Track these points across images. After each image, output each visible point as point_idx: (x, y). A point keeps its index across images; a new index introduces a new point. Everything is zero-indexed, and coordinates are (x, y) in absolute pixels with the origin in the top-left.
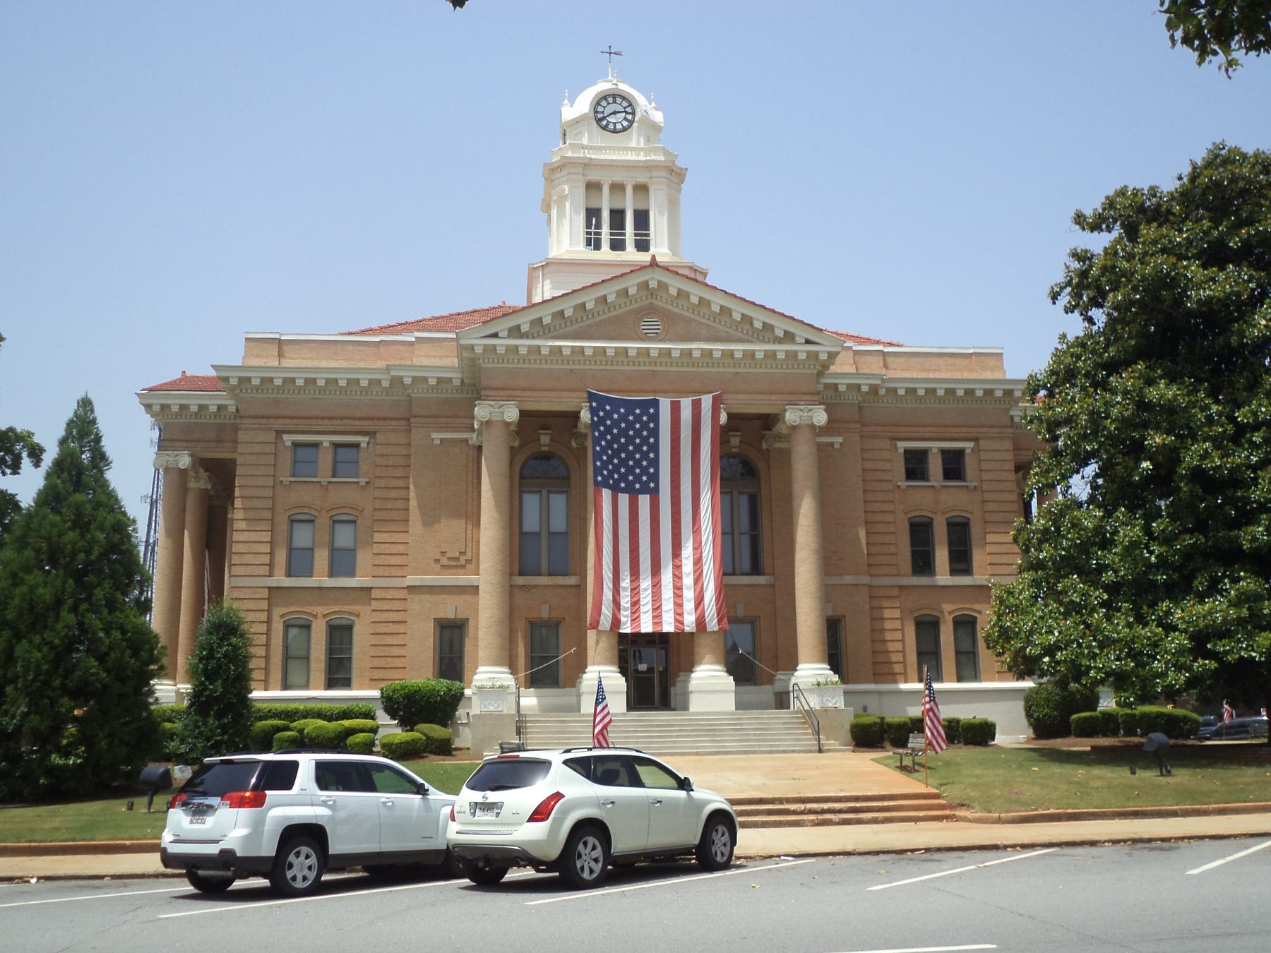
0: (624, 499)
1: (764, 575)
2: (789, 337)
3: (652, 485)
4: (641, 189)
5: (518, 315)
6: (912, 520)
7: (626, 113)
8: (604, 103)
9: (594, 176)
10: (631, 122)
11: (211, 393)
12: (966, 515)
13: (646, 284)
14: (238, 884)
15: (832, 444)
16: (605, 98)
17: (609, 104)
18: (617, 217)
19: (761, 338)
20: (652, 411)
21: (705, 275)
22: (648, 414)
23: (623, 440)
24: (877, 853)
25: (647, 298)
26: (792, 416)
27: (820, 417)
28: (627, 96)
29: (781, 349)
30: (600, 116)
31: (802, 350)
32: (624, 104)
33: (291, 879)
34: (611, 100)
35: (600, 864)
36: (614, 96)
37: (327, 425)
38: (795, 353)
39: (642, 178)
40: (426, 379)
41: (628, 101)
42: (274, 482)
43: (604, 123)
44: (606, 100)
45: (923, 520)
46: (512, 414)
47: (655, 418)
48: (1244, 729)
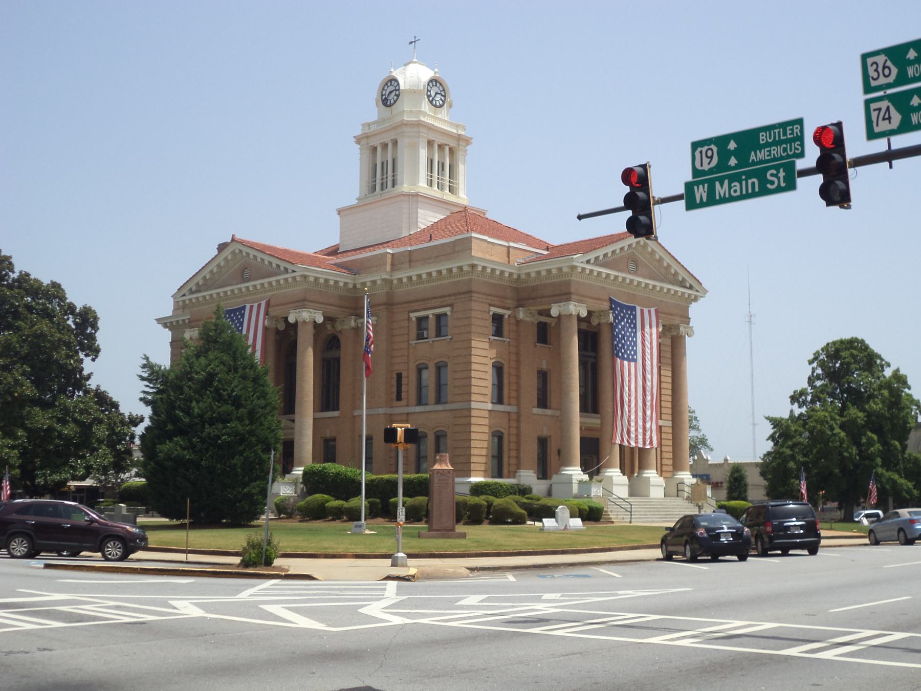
1: (550, 409)
2: (691, 287)
10: (444, 102)
11: (332, 272)
16: (386, 84)
21: (484, 214)
34: (434, 83)
39: (452, 143)
42: (409, 338)
44: (436, 83)
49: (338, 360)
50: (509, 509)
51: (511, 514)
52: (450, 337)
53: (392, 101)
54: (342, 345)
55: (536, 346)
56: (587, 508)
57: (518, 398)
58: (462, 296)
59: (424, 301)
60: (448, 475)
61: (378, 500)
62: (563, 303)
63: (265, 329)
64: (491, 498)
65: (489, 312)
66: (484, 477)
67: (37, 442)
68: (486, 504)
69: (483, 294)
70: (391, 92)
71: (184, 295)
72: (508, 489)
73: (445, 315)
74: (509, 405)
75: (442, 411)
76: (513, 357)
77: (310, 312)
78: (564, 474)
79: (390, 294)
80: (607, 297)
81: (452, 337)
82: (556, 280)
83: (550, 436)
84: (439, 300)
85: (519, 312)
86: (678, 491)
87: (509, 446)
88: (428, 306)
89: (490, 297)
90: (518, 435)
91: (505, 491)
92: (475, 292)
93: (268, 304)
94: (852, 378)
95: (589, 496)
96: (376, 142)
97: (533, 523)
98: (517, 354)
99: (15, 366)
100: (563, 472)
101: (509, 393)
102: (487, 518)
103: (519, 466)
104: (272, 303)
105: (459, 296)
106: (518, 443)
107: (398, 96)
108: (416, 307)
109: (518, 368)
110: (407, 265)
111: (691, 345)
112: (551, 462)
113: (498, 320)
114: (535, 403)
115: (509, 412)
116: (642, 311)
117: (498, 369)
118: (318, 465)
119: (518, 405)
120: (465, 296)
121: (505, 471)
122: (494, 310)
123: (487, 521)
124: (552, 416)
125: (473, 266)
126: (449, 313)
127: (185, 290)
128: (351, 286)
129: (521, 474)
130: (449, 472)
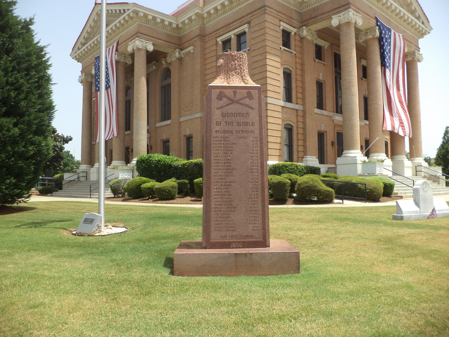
1: (326, 110)
49: (169, 85)
50: (315, 187)
51: (318, 192)
52: (248, 48)
54: (171, 76)
55: (315, 61)
56: (382, 185)
57: (303, 99)
58: (257, 12)
59: (227, 27)
60: (247, 101)
61: (187, 181)
62: (343, 13)
63: (117, 62)
64: (293, 176)
65: (280, 27)
66: (279, 161)
68: (289, 182)
69: (275, 10)
71: (76, 52)
72: (302, 170)
73: (244, 33)
74: (297, 104)
76: (299, 66)
77: (142, 42)
78: (348, 156)
79: (202, 29)
80: (373, 16)
81: (250, 48)
83: (326, 131)
85: (303, 31)
86: (416, 171)
87: (297, 137)
88: (230, 29)
89: (280, 14)
90: (304, 129)
91: (300, 171)
92: (268, 7)
95: (373, 174)
97: (341, 201)
98: (302, 64)
99: (395, 232)
100: (348, 155)
101: (297, 94)
102: (291, 197)
103: (305, 153)
105: (255, 13)
106: (304, 134)
109: (303, 76)
111: (420, 66)
112: (327, 151)
113: (286, 35)
114: (315, 105)
115: (297, 110)
117: (287, 76)
119: (304, 105)
120: (260, 11)
121: (295, 157)
122: (284, 25)
123: (291, 200)
124: (327, 116)
126: (247, 30)
128: (174, 26)
129: (308, 159)
130: (250, 96)
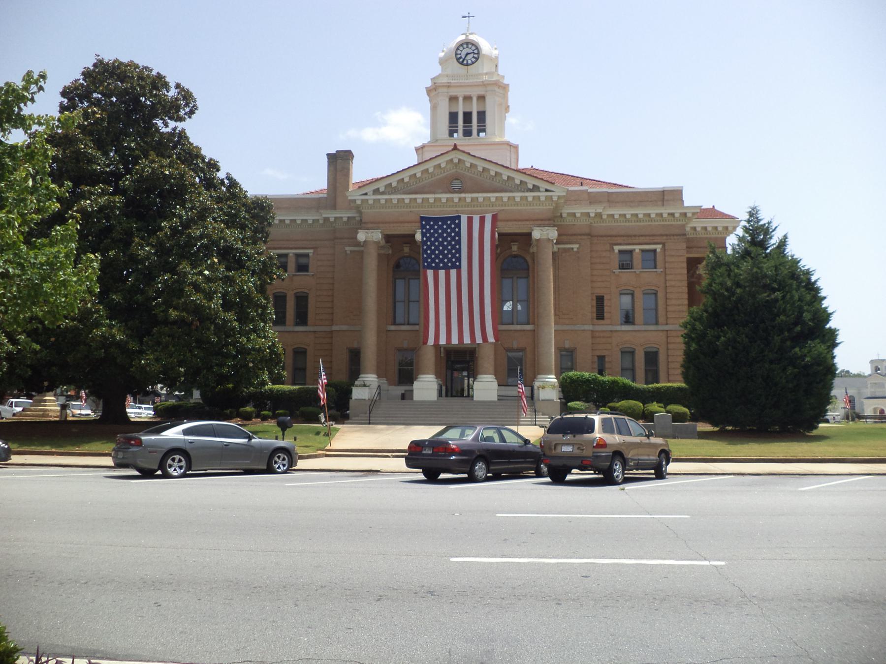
0: (442, 273)
2: (536, 188)
3: (457, 264)
4: (481, 98)
5: (377, 183)
6: (298, 295)
7: (474, 54)
8: (461, 48)
9: (453, 92)
12: (285, 291)
13: (451, 160)
14: (443, 476)
15: (573, 249)
16: (462, 45)
17: (464, 48)
18: (468, 116)
19: (520, 189)
20: (457, 221)
22: (454, 223)
23: (441, 248)
24: (738, 474)
25: (453, 169)
26: (536, 234)
27: (553, 234)
28: (474, 43)
29: (530, 195)
30: (459, 56)
31: (542, 195)
32: (473, 48)
33: (169, 465)
34: (465, 46)
35: (175, 456)
36: (467, 44)
37: (642, 239)
38: (539, 197)
40: (341, 218)
41: (475, 46)
43: (465, 62)
45: (282, 294)
46: (376, 236)
47: (459, 226)
48: (373, 401)
53: (470, 62)
59: (630, 237)
67: (150, 342)
70: (467, 54)
75: (654, 331)
82: (713, 236)
84: (648, 238)
88: (634, 241)
93: (495, 218)
94: (82, 338)
96: (460, 93)
104: (500, 217)
107: (477, 59)
108: (619, 242)
110: (660, 203)
116: (470, 220)
118: (588, 374)
125: (684, 215)
127: (369, 189)
